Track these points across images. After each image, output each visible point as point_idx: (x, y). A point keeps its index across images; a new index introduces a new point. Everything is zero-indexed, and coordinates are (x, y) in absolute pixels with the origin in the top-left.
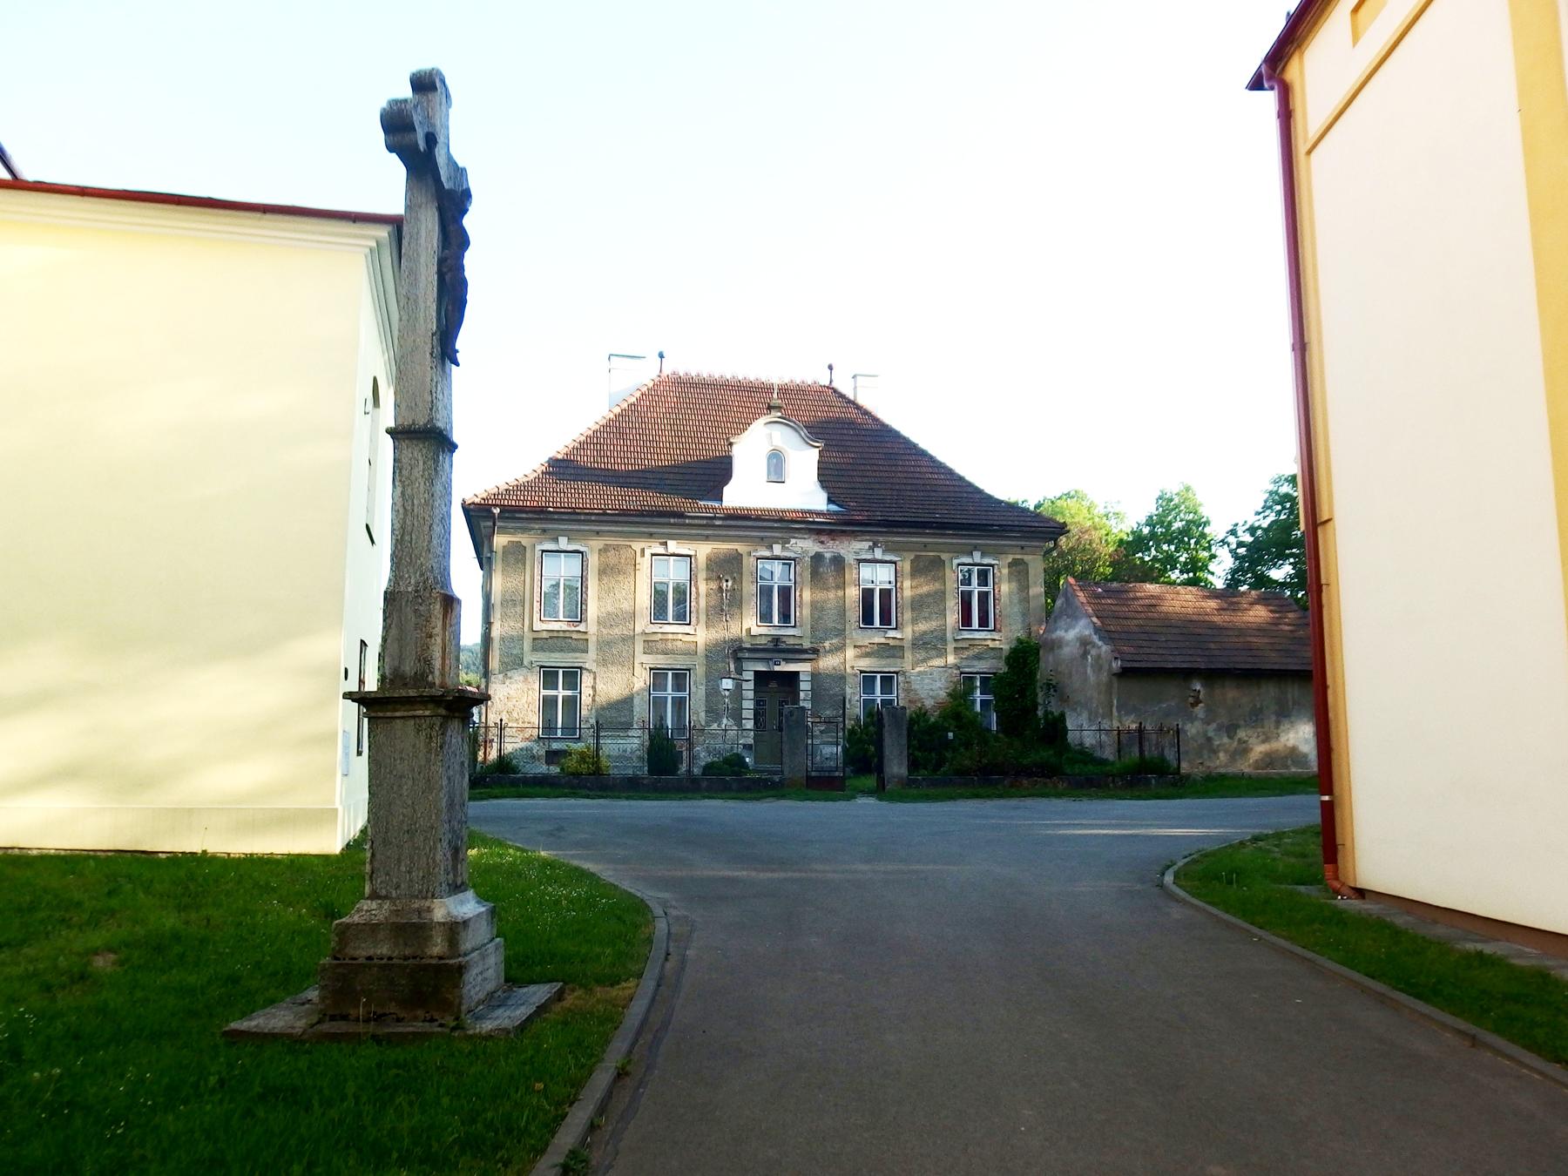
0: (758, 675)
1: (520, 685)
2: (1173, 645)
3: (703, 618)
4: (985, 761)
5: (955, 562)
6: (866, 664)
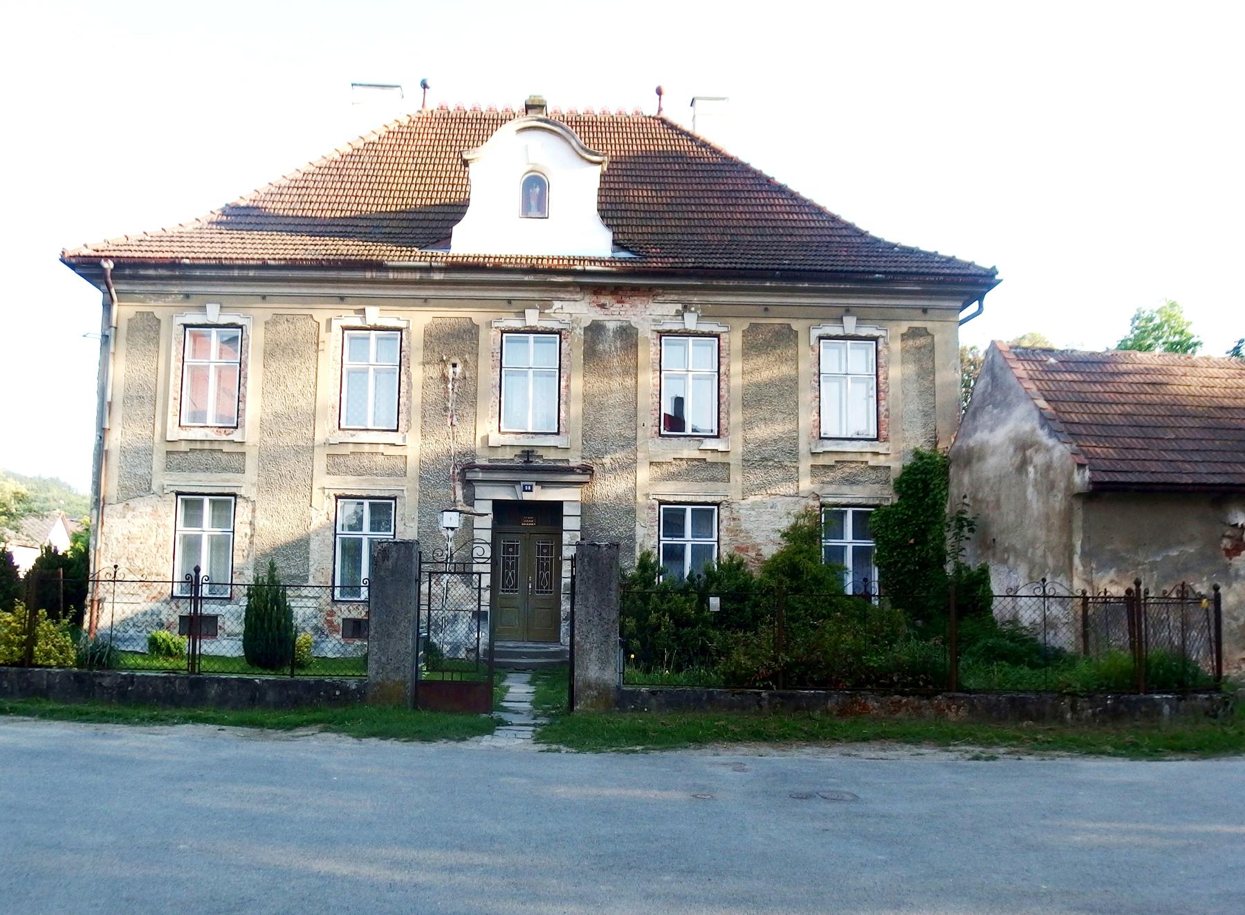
0: (498, 505)
1: (147, 520)
2: (1190, 445)
3: (417, 420)
4: (785, 658)
5: (815, 333)
6: (673, 491)
